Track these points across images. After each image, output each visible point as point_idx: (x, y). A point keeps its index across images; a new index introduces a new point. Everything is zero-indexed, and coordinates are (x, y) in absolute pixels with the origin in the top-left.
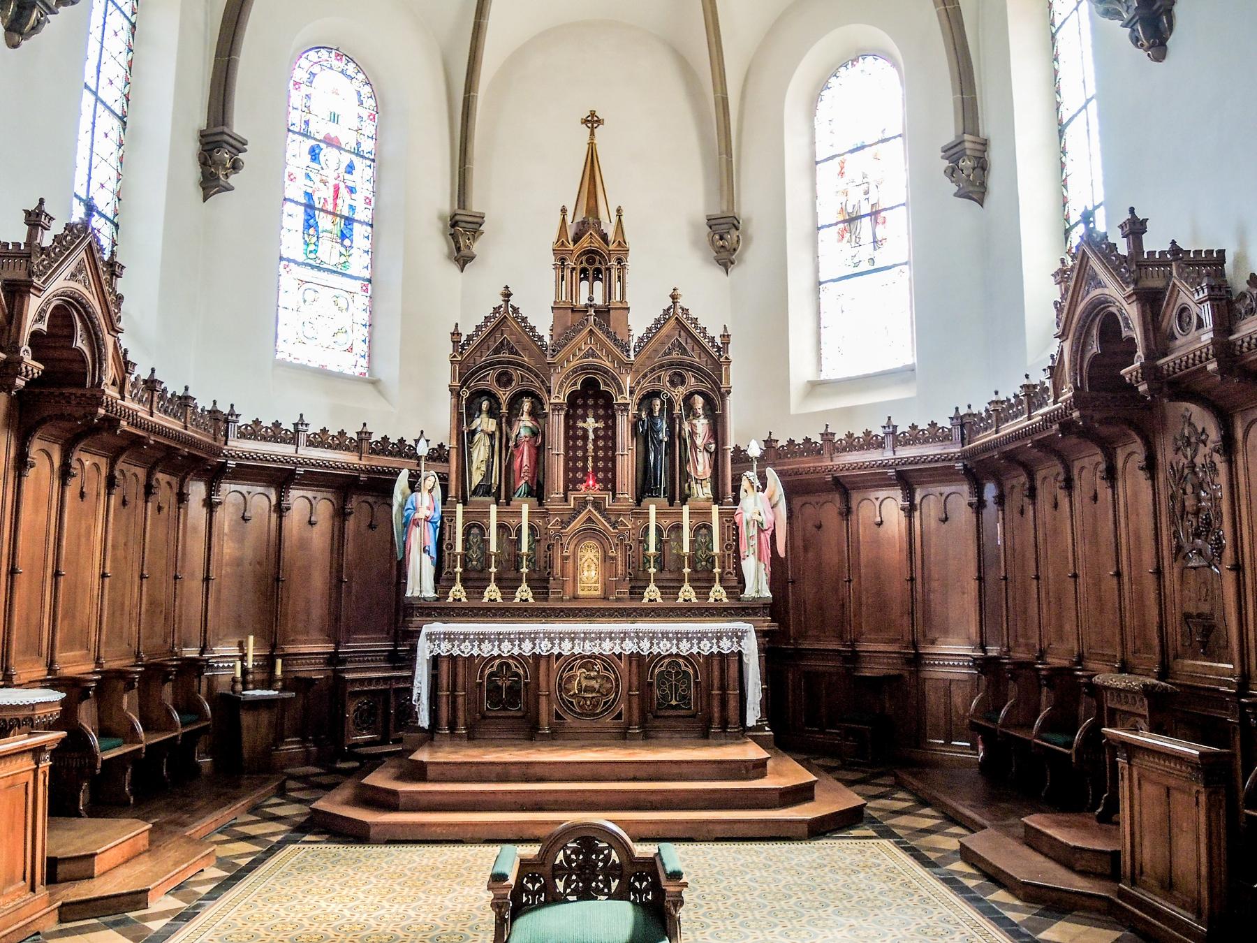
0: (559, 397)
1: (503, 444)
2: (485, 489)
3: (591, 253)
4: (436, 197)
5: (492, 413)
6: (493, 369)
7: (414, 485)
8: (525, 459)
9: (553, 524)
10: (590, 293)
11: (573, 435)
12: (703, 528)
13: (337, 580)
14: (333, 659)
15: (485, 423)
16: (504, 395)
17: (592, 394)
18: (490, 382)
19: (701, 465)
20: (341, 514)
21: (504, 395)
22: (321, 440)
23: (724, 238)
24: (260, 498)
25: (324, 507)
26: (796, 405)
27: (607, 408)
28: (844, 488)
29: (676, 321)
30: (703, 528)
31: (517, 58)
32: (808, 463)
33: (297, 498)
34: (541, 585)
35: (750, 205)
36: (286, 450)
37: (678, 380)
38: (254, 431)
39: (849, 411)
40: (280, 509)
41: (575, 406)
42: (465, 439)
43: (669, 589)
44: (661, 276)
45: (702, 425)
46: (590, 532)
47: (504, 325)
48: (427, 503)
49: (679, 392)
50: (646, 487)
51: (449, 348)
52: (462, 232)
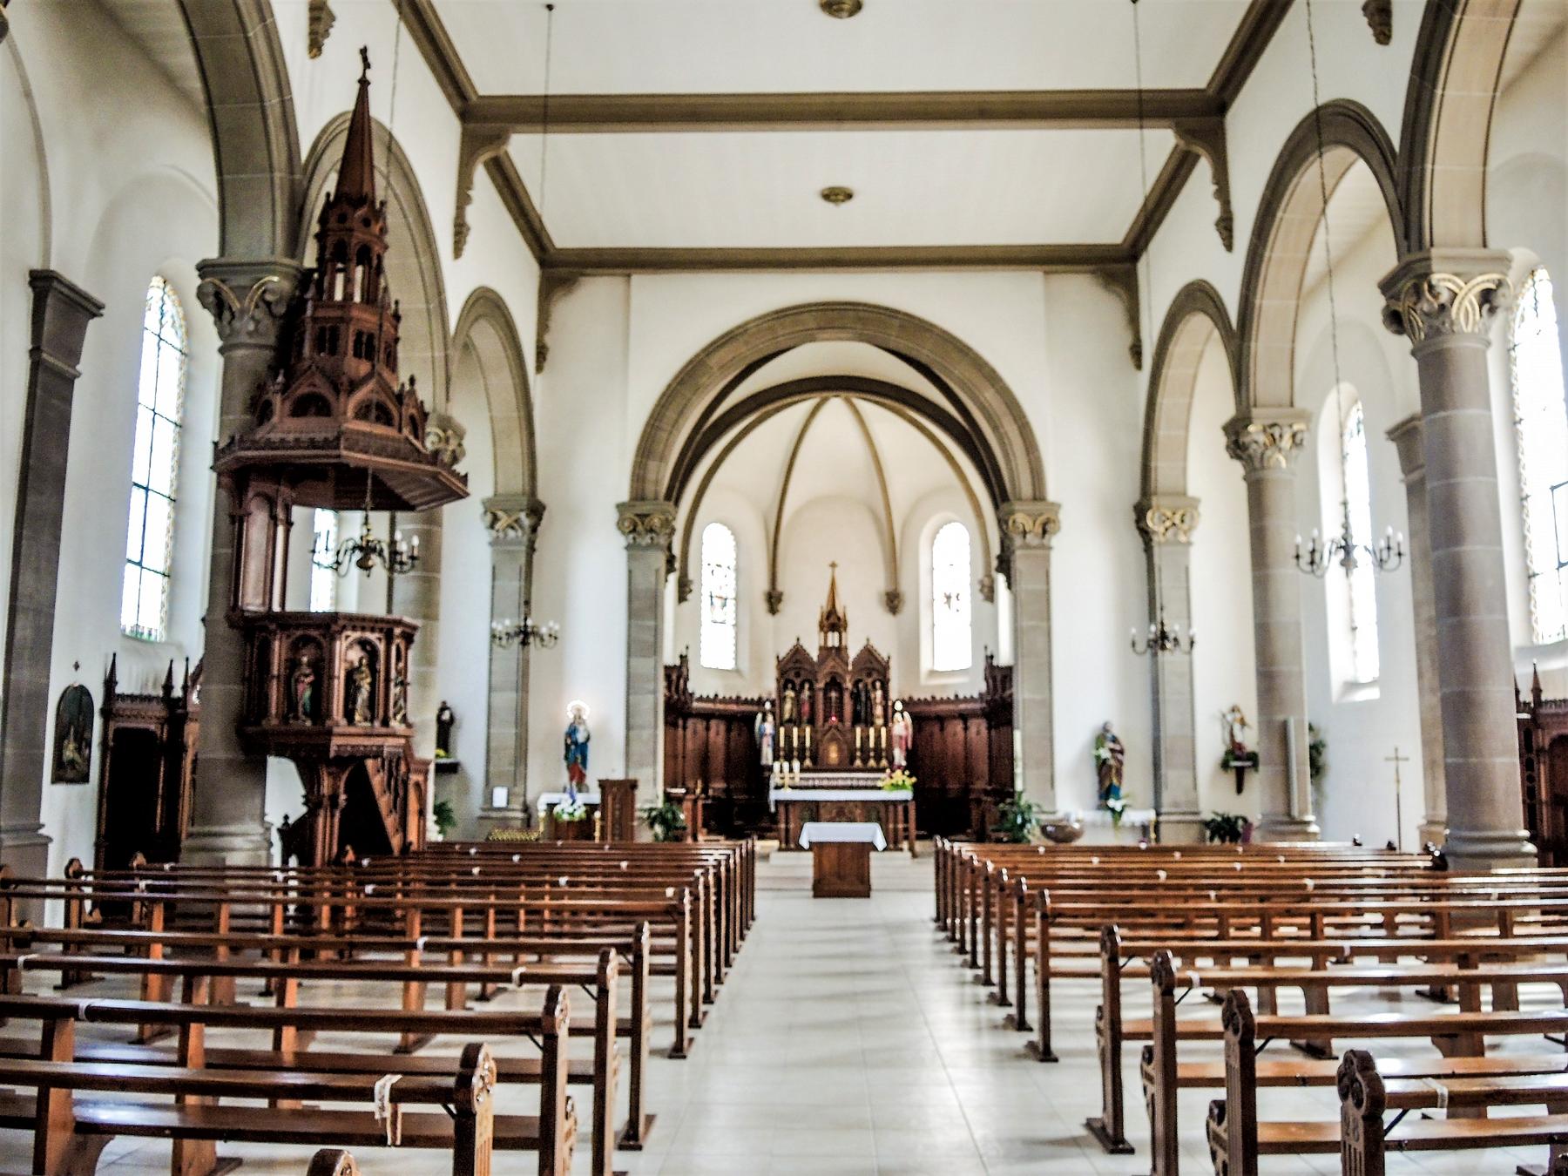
0: (821, 685)
1: (797, 701)
2: (790, 720)
3: (833, 622)
4: (763, 585)
5: (793, 689)
6: (794, 669)
7: (764, 720)
8: (806, 708)
9: (819, 736)
10: (833, 640)
11: (827, 699)
12: (878, 738)
13: (728, 759)
14: (726, 791)
15: (790, 693)
16: (798, 681)
17: (834, 683)
18: (791, 675)
19: (879, 711)
20: (728, 730)
21: (798, 681)
22: (724, 701)
23: (893, 601)
24: (700, 725)
25: (722, 728)
26: (924, 680)
27: (840, 690)
28: (941, 719)
29: (868, 653)
30: (878, 738)
31: (798, 513)
32: (926, 709)
33: (713, 723)
34: (814, 759)
35: (905, 587)
36: (710, 706)
37: (869, 675)
38: (701, 699)
39: (944, 687)
40: (708, 729)
41: (828, 687)
42: (782, 699)
43: (865, 760)
44: (867, 629)
45: (879, 693)
46: (834, 739)
47: (798, 653)
48: (769, 727)
49: (869, 681)
50: (856, 720)
51: (775, 663)
52: (774, 600)
